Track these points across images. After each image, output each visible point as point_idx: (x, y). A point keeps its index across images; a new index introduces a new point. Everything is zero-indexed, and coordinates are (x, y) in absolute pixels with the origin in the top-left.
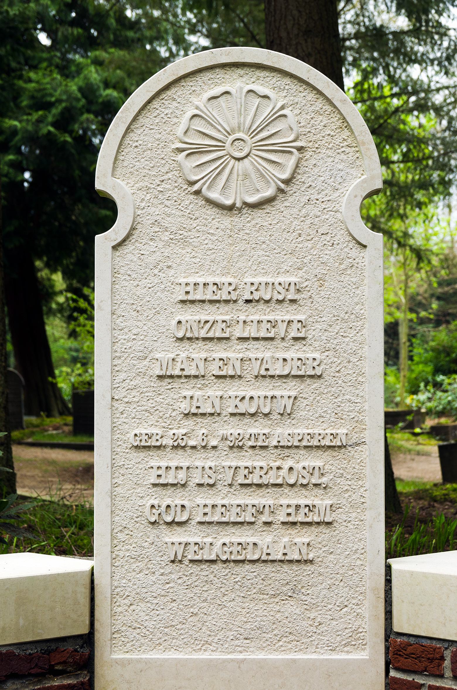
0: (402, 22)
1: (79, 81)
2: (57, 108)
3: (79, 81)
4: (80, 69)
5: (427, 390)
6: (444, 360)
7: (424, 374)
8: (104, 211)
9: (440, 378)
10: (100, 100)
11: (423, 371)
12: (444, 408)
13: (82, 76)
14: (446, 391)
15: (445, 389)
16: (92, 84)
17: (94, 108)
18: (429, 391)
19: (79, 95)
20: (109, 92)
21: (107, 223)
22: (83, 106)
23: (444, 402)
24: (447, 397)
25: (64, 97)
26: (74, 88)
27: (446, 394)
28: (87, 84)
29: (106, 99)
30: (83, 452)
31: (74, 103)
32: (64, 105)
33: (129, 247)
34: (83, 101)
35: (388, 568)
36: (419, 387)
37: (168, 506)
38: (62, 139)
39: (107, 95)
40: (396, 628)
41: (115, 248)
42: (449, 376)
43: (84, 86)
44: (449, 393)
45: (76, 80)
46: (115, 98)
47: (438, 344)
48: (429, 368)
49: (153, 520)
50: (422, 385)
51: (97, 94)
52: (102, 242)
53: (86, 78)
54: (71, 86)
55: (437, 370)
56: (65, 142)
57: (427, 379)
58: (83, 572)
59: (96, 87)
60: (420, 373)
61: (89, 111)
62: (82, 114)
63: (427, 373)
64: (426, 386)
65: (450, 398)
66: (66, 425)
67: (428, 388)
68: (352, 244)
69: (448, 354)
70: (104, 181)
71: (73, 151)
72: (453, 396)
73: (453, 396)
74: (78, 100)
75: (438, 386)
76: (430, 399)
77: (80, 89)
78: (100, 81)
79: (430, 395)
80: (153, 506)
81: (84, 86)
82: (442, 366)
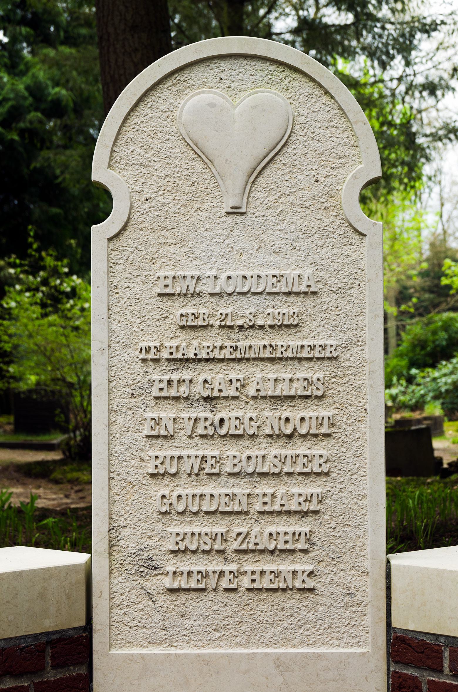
0: (348, 18)
1: (27, 80)
2: (3, 107)
3: (27, 80)
4: (28, 67)
5: (399, 383)
6: (419, 353)
7: (398, 368)
8: (98, 203)
9: (414, 371)
10: (50, 98)
11: (398, 365)
12: (417, 402)
13: (30, 74)
14: (419, 385)
15: (419, 382)
16: (40, 83)
17: (43, 106)
18: (402, 385)
19: (26, 94)
20: (57, 89)
21: (101, 213)
22: (31, 105)
23: (418, 395)
24: (420, 390)
25: (12, 96)
26: (21, 87)
27: (419, 388)
28: (35, 83)
29: (55, 97)
30: (27, 452)
31: (21, 102)
32: (10, 103)
33: (124, 239)
34: (31, 99)
35: (388, 562)
36: (392, 381)
37: (179, 496)
38: (9, 137)
39: (56, 94)
40: (395, 624)
41: (110, 240)
42: (422, 369)
43: (32, 84)
44: (422, 387)
45: (24, 79)
46: (64, 95)
47: (413, 338)
48: (404, 362)
49: (164, 509)
50: (395, 379)
51: (46, 92)
52: (99, 233)
53: (34, 76)
54: (18, 85)
55: (413, 364)
56: (12, 140)
57: (402, 373)
58: (79, 565)
59: (44, 85)
60: (394, 367)
61: (36, 110)
62: (30, 112)
63: (402, 367)
64: (398, 380)
65: (422, 392)
66: (9, 423)
67: (401, 382)
68: (351, 233)
69: (423, 348)
70: (99, 173)
71: (21, 149)
72: (426, 390)
73: (426, 390)
74: (25, 98)
75: (410, 380)
76: (404, 393)
77: (27, 88)
78: (49, 79)
79: (402, 389)
80: (164, 496)
81: (32, 84)
82: (417, 359)
